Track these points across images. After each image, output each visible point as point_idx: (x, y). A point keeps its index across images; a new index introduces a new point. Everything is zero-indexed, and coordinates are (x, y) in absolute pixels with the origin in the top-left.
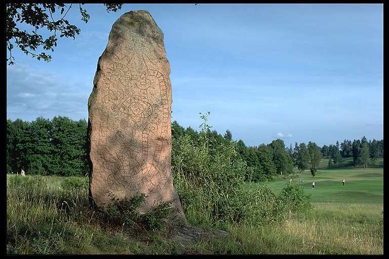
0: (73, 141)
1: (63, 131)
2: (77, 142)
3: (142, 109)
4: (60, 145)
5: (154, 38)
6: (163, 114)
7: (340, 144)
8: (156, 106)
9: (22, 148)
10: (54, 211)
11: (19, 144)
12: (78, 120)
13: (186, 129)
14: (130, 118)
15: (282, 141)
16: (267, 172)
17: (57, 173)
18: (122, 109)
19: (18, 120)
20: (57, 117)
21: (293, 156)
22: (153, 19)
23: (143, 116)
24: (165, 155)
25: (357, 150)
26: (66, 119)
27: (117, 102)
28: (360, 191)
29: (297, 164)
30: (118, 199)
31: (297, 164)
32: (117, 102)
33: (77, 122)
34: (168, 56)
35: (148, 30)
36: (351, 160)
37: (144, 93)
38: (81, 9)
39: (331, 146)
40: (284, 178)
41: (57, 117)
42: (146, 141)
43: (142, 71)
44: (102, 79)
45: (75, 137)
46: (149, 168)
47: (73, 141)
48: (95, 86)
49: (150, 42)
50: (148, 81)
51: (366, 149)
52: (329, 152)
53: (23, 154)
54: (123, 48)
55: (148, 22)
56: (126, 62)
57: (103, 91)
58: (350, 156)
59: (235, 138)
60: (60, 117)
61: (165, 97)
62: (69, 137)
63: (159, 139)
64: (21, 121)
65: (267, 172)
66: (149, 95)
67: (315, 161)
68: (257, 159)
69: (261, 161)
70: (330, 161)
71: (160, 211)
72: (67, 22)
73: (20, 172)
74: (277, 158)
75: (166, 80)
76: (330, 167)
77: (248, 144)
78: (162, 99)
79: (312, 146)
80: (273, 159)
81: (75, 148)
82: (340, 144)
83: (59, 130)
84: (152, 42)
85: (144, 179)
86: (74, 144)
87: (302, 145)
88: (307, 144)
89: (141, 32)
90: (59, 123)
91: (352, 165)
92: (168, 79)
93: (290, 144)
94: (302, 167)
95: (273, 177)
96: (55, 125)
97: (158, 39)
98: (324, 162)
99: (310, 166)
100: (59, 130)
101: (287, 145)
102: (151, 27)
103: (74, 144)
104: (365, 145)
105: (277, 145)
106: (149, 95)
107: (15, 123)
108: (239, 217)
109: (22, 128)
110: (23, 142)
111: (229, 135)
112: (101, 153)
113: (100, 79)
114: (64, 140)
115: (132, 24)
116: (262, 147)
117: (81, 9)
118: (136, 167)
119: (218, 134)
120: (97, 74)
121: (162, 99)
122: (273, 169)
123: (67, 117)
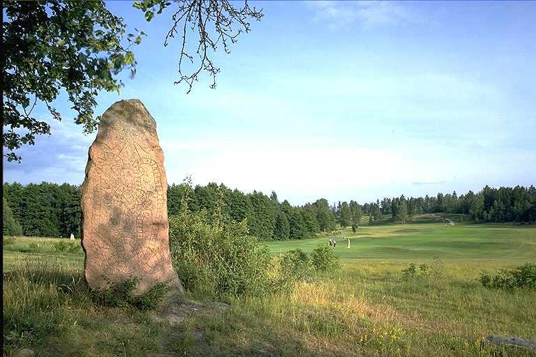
3: (135, 196)
5: (146, 127)
7: (380, 201)
9: (70, 212)
10: (53, 290)
11: (67, 208)
13: (233, 191)
14: (123, 205)
15: (325, 200)
16: (311, 229)
19: (65, 184)
21: (335, 214)
22: (145, 108)
23: (137, 203)
24: (165, 233)
25: (396, 207)
28: (395, 247)
29: (340, 221)
31: (340, 221)
34: (162, 144)
35: (140, 119)
36: (390, 216)
37: (137, 181)
38: (49, 107)
39: (372, 204)
40: (327, 235)
44: (92, 169)
46: (152, 244)
48: (87, 176)
49: (142, 131)
51: (404, 207)
52: (370, 209)
53: (72, 218)
54: (114, 137)
55: (139, 111)
58: (388, 213)
59: (281, 200)
61: (159, 184)
63: (154, 224)
64: (68, 185)
65: (311, 229)
67: (356, 218)
68: (302, 219)
69: (305, 220)
70: (371, 218)
71: (158, 289)
72: (34, 120)
73: (69, 237)
74: (320, 216)
75: (160, 167)
76: (371, 224)
77: (293, 204)
79: (354, 204)
80: (318, 217)
82: (380, 201)
84: (145, 131)
85: (146, 256)
87: (345, 203)
88: (349, 203)
89: (130, 120)
91: (391, 222)
92: (162, 166)
93: (333, 202)
94: (344, 224)
95: (317, 234)
97: (150, 127)
98: (365, 218)
99: (351, 223)
101: (331, 204)
102: (143, 115)
104: (404, 203)
105: (322, 203)
107: (61, 187)
108: (242, 290)
109: (70, 192)
110: (72, 206)
111: (274, 196)
115: (121, 113)
116: (307, 206)
117: (49, 107)
118: (137, 246)
119: (264, 195)
120: (88, 163)
122: (316, 227)
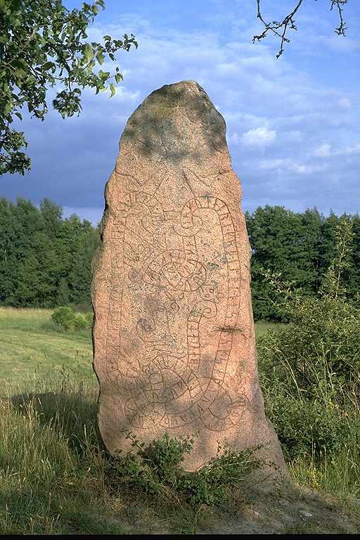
0: (294, 253)
1: (275, 235)
2: (302, 254)
4: (269, 261)
6: (228, 281)
8: (214, 266)
12: (302, 212)
17: (266, 317)
18: (147, 277)
20: (263, 208)
26: (279, 210)
27: (138, 265)
30: (142, 445)
32: (138, 265)
33: (301, 215)
37: (189, 244)
41: (263, 208)
42: (196, 334)
43: (183, 201)
45: (297, 246)
47: (294, 253)
50: (196, 220)
56: (153, 188)
57: (114, 246)
60: (268, 208)
61: (232, 248)
62: (288, 245)
66: (200, 247)
78: (226, 253)
81: (299, 267)
83: (268, 231)
86: (297, 259)
90: (268, 218)
96: (259, 224)
100: (268, 231)
103: (297, 259)
106: (200, 247)
112: (113, 361)
113: (108, 225)
114: (279, 252)
121: (226, 253)
123: (280, 205)
